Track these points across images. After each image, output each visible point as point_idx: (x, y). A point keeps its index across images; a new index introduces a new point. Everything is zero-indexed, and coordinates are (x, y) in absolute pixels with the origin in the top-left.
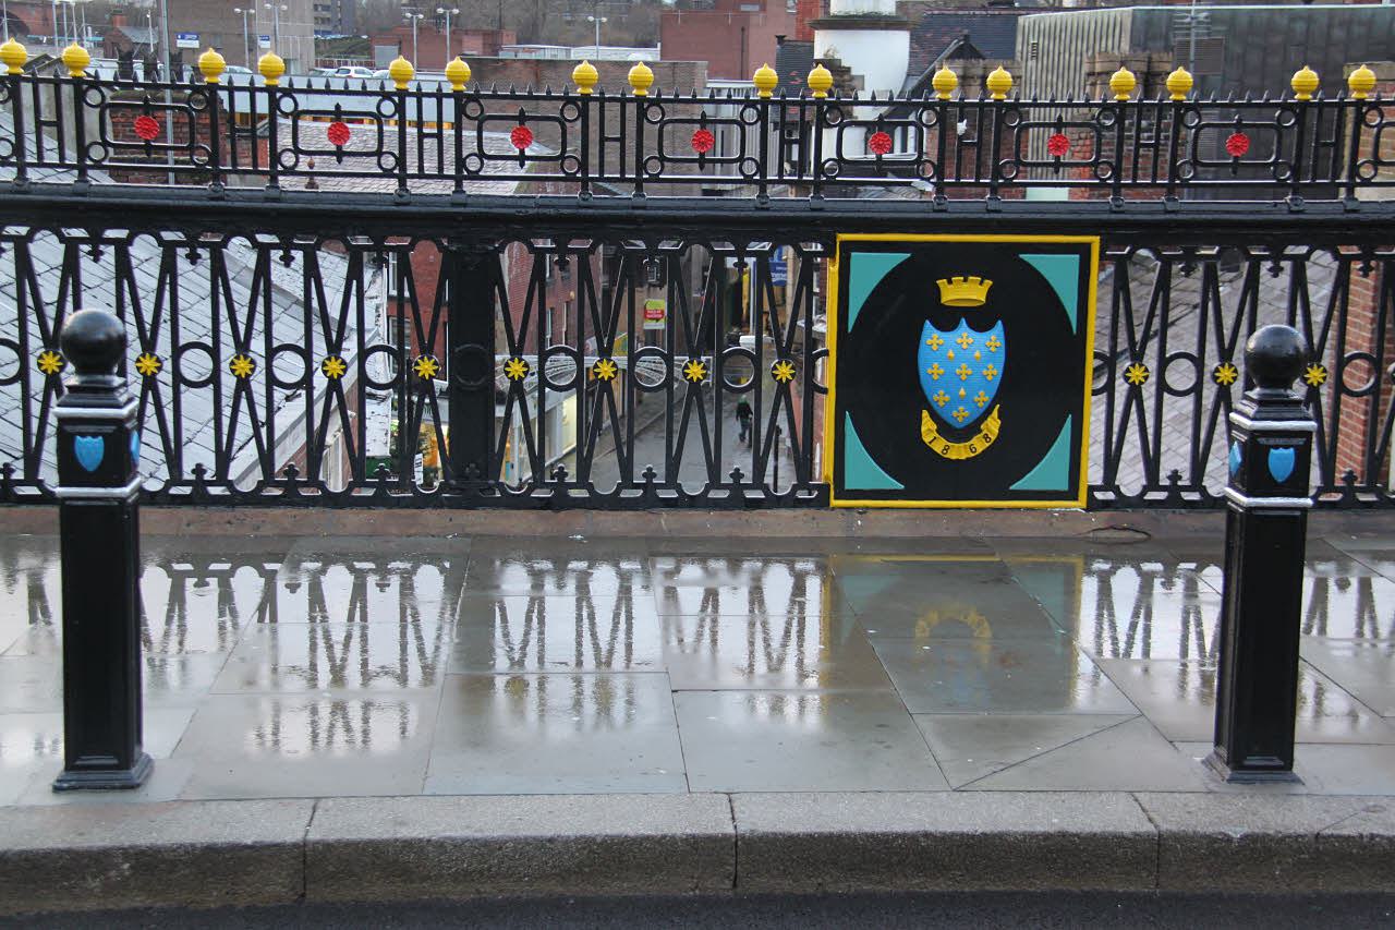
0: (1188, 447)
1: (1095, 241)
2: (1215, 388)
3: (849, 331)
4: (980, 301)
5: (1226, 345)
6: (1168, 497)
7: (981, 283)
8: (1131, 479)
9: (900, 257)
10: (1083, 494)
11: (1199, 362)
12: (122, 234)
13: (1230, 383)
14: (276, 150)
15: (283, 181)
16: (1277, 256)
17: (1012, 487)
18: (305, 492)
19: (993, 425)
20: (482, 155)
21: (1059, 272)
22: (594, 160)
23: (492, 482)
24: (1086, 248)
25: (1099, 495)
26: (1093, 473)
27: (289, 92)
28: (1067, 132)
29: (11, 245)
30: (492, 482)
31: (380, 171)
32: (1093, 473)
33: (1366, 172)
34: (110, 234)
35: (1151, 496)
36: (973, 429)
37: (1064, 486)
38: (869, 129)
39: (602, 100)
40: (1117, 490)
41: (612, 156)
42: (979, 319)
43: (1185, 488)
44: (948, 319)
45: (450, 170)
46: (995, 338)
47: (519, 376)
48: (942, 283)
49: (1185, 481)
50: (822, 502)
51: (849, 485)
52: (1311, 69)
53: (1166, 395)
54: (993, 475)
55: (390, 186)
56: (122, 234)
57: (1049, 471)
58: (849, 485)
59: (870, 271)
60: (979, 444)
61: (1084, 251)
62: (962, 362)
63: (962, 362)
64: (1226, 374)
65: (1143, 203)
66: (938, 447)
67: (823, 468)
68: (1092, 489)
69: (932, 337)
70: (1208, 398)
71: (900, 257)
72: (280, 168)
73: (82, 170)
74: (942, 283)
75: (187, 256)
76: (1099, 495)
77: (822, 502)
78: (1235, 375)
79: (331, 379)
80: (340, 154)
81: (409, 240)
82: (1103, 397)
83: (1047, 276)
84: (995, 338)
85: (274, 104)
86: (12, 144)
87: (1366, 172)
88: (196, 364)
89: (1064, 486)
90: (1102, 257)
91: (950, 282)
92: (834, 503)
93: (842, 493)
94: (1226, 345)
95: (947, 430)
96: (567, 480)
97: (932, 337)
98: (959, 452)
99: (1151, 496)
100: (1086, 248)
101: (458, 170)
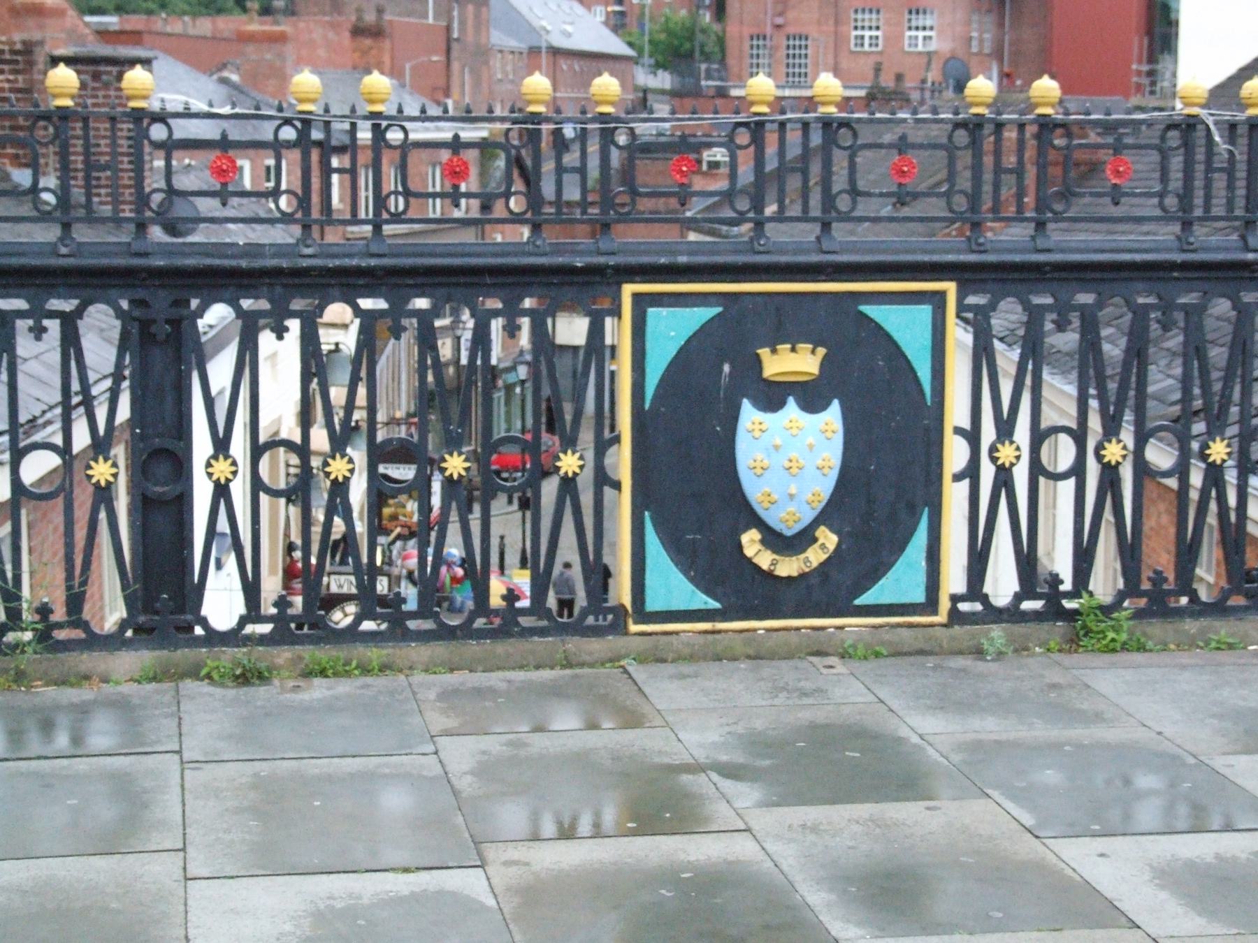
0: (60, 575)
1: (950, 287)
2: (210, 487)
3: (647, 406)
4: (811, 374)
5: (221, 434)
6: (274, 629)
7: (813, 352)
8: (1002, 582)
9: (704, 314)
10: (945, 605)
11: (1079, 437)
12: (68, 305)
13: (228, 480)
14: (380, 192)
15: (388, 229)
16: (38, 313)
17: (857, 602)
18: (525, 621)
19: (828, 539)
20: (275, 193)
21: (907, 326)
22: (1198, 201)
23: (189, 617)
24: (942, 295)
25: (964, 607)
26: (954, 579)
27: (399, 118)
28: (914, 156)
29: (415, 321)
30: (189, 617)
31: (35, 213)
32: (954, 579)
33: (397, 204)
34: (55, 304)
35: (1027, 605)
36: (805, 539)
37: (919, 596)
38: (482, 153)
39: (999, 126)
40: (984, 599)
41: (1007, 192)
42: (811, 396)
43: (413, 615)
44: (772, 396)
45: (816, 211)
46: (833, 416)
47: (345, 477)
48: (764, 352)
49: (59, 614)
50: (618, 628)
51: (652, 605)
52: (312, 72)
53: (1042, 480)
54: (831, 592)
55: (47, 234)
56: (68, 305)
57: (902, 581)
58: (652, 605)
59: (672, 329)
60: (815, 556)
61: (938, 300)
62: (790, 456)
63: (790, 456)
64: (1006, 453)
65: (1008, 239)
66: (764, 560)
67: (622, 591)
68: (955, 599)
69: (749, 415)
70: (83, 503)
71: (704, 314)
72: (385, 216)
73: (141, 227)
74: (764, 352)
75: (31, 329)
76: (964, 607)
77: (618, 628)
78: (350, 466)
79: (217, 484)
80: (223, 195)
81: (76, 302)
82: (965, 484)
83: (896, 336)
84: (833, 416)
85: (378, 132)
86: (524, 194)
87: (843, 203)
88: (1063, 453)
89: (919, 596)
90: (961, 308)
91: (793, 350)
92: (634, 628)
93: (643, 616)
94: (221, 434)
95: (777, 541)
96: (1062, 588)
97: (749, 415)
98: (788, 567)
99: (1027, 605)
100: (942, 295)
101: (825, 210)
